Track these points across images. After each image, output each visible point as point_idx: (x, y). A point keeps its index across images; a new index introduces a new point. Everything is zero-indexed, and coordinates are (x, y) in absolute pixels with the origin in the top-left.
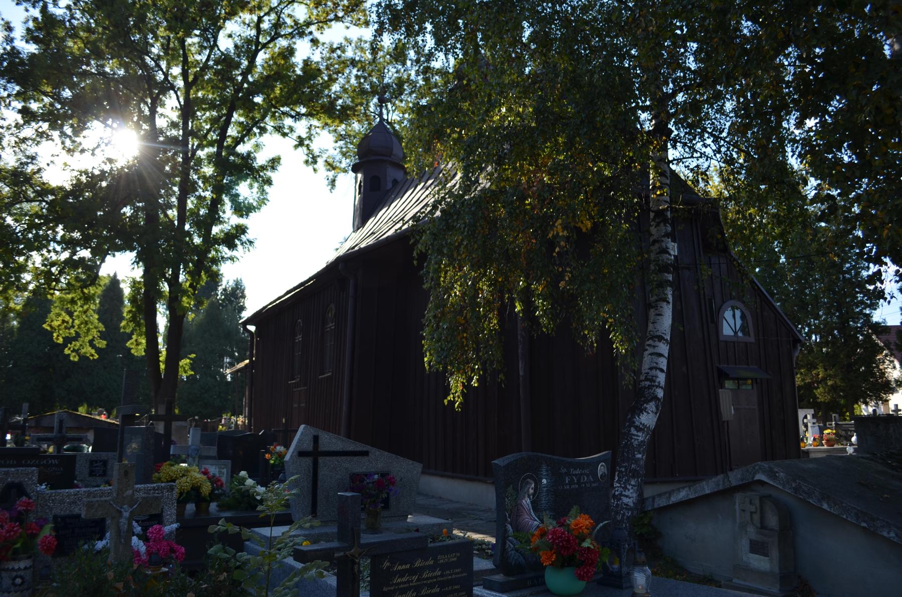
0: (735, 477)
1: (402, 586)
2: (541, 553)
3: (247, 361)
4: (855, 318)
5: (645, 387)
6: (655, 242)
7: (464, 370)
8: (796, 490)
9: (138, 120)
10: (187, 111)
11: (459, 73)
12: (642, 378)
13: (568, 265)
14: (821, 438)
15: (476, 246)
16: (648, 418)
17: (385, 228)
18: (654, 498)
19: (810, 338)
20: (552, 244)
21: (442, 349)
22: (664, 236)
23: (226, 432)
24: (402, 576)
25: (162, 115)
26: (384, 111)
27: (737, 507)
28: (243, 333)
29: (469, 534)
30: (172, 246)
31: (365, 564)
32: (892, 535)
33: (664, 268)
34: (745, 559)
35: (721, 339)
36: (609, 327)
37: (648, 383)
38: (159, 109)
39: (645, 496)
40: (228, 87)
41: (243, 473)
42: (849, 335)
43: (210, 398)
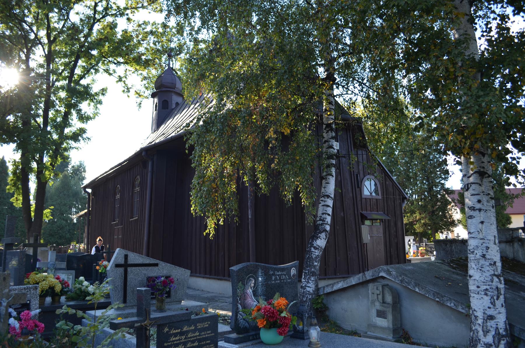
0: (369, 275)
1: (176, 342)
2: (258, 320)
3: (86, 211)
4: (436, 186)
5: (319, 225)
6: (326, 141)
7: (216, 215)
8: (402, 281)
9: (19, 62)
10: (50, 58)
11: (215, 41)
12: (318, 219)
13: (277, 154)
14: (418, 252)
15: (224, 142)
16: (321, 242)
17: (170, 131)
18: (324, 287)
19: (412, 196)
20: (267, 143)
21: (203, 203)
22: (331, 138)
23: (72, 253)
24: (175, 336)
25: (33, 59)
26: (171, 63)
27: (370, 292)
28: (84, 194)
29: (217, 311)
30: (39, 140)
31: (153, 331)
32: (452, 305)
33: (331, 157)
34: (374, 320)
35: (363, 197)
36: (300, 190)
37: (321, 222)
38: (32, 56)
39: (319, 286)
40: (75, 44)
41: (82, 278)
42: (433, 195)
43: (61, 234)
